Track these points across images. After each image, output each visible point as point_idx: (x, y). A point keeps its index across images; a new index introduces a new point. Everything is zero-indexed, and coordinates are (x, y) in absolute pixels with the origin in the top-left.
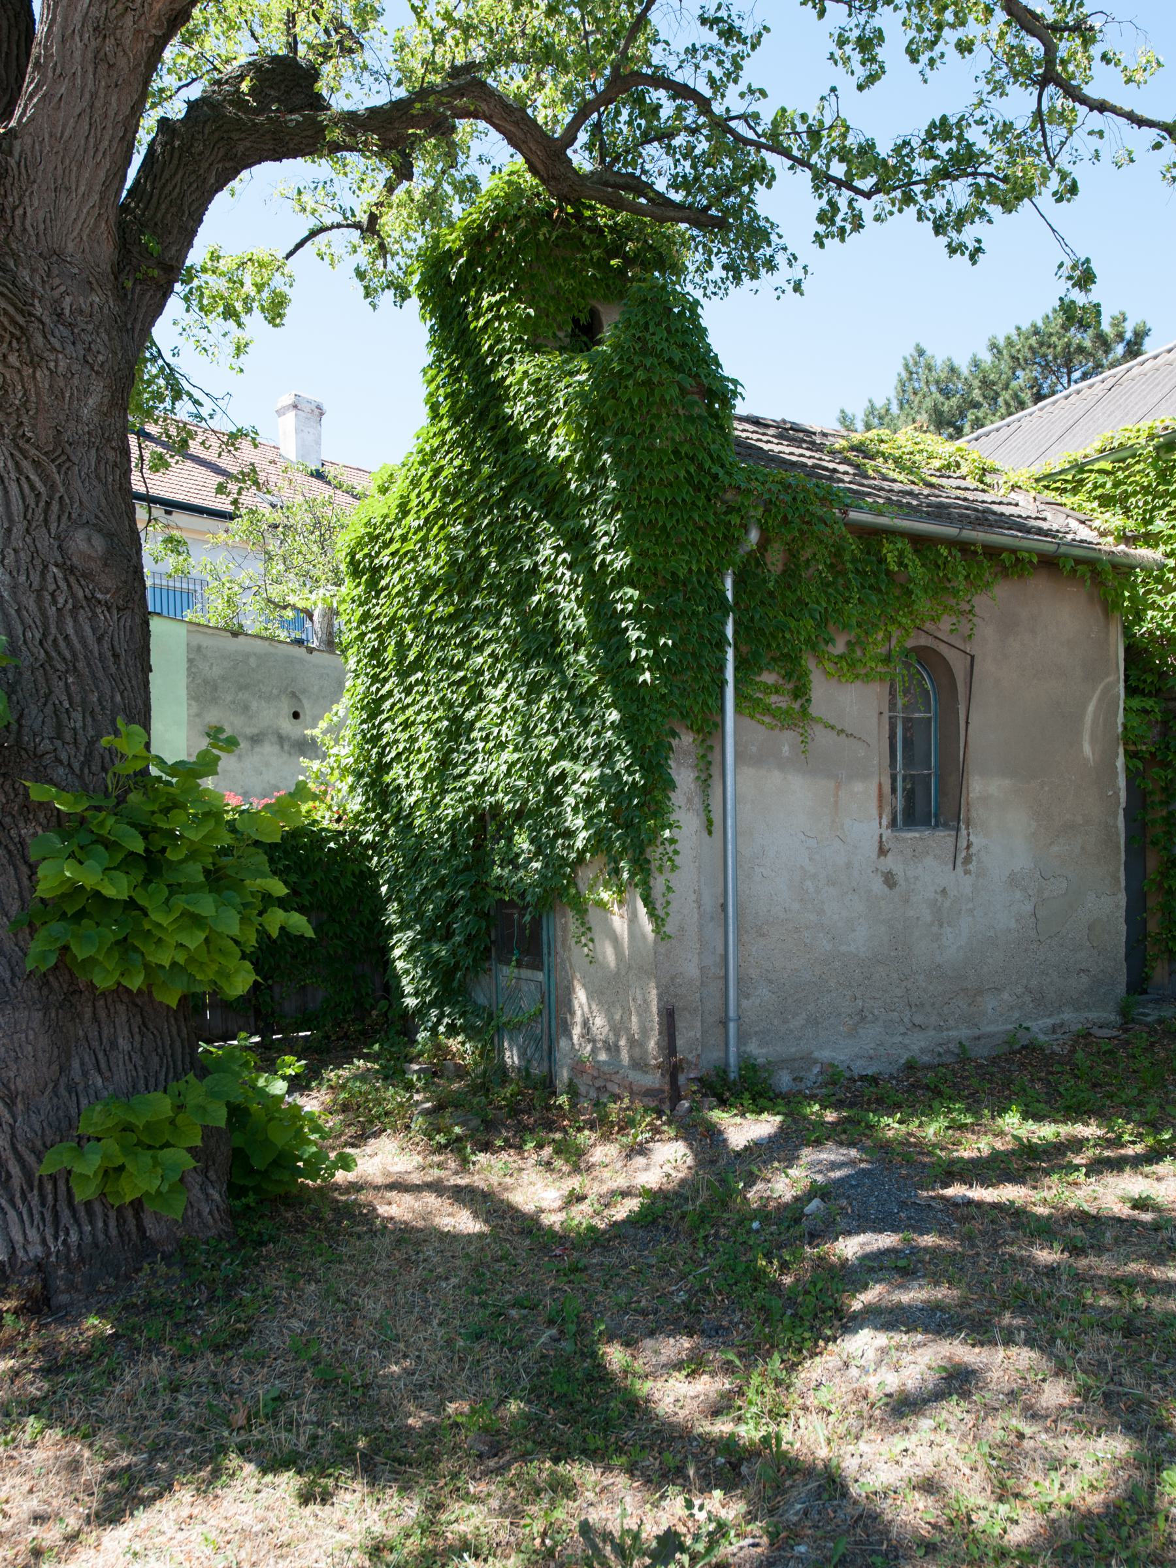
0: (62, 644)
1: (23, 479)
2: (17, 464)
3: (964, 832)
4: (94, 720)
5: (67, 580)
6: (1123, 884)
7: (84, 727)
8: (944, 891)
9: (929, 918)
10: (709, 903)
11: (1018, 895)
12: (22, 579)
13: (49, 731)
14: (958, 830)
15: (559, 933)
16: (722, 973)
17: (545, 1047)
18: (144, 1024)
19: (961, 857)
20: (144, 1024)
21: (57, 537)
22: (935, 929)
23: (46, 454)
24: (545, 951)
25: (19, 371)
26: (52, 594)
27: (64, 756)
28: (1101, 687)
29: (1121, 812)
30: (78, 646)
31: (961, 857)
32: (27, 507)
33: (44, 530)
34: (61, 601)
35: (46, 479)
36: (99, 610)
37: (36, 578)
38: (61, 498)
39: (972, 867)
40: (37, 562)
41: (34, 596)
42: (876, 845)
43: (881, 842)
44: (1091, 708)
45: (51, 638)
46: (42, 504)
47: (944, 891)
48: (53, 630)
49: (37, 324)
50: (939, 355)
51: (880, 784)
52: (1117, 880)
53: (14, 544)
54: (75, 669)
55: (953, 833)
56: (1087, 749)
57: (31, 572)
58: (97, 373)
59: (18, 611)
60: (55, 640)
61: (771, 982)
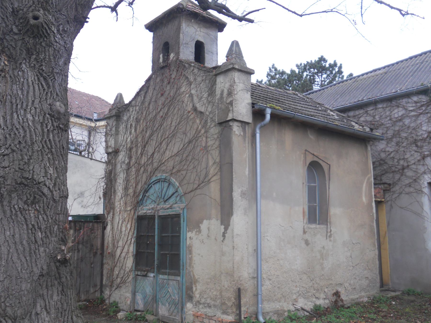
0: (48, 142)
1: (40, 83)
2: (38, 78)
3: (329, 226)
4: (57, 171)
5: (51, 120)
6: (377, 247)
7: (54, 173)
8: (323, 247)
9: (319, 257)
10: (251, 249)
11: (346, 249)
12: (37, 118)
13: (43, 174)
14: (327, 225)
15: (188, 261)
16: (256, 276)
17: (180, 307)
18: (63, 290)
19: (329, 235)
20: (63, 290)
21: (50, 104)
22: (321, 261)
23: (48, 76)
24: (181, 268)
25: (45, 48)
26: (46, 125)
27: (47, 183)
28: (367, 178)
29: (375, 221)
30: (53, 143)
31: (329, 235)
32: (40, 94)
33: (45, 102)
34: (49, 127)
35: (48, 84)
36: (60, 131)
37: (41, 118)
38: (51, 91)
39: (332, 239)
40: (42, 112)
41: (40, 124)
42: (302, 230)
43: (304, 229)
44: (364, 185)
45: (44, 140)
46: (45, 93)
47: (323, 247)
48: (46, 137)
49: (52, 33)
50: (280, 68)
51: (303, 209)
52: (375, 245)
53: (35, 106)
54: (51, 152)
55: (326, 226)
56: (364, 199)
57: (40, 116)
58: (66, 50)
59: (34, 130)
60: (45, 141)
61: (270, 280)
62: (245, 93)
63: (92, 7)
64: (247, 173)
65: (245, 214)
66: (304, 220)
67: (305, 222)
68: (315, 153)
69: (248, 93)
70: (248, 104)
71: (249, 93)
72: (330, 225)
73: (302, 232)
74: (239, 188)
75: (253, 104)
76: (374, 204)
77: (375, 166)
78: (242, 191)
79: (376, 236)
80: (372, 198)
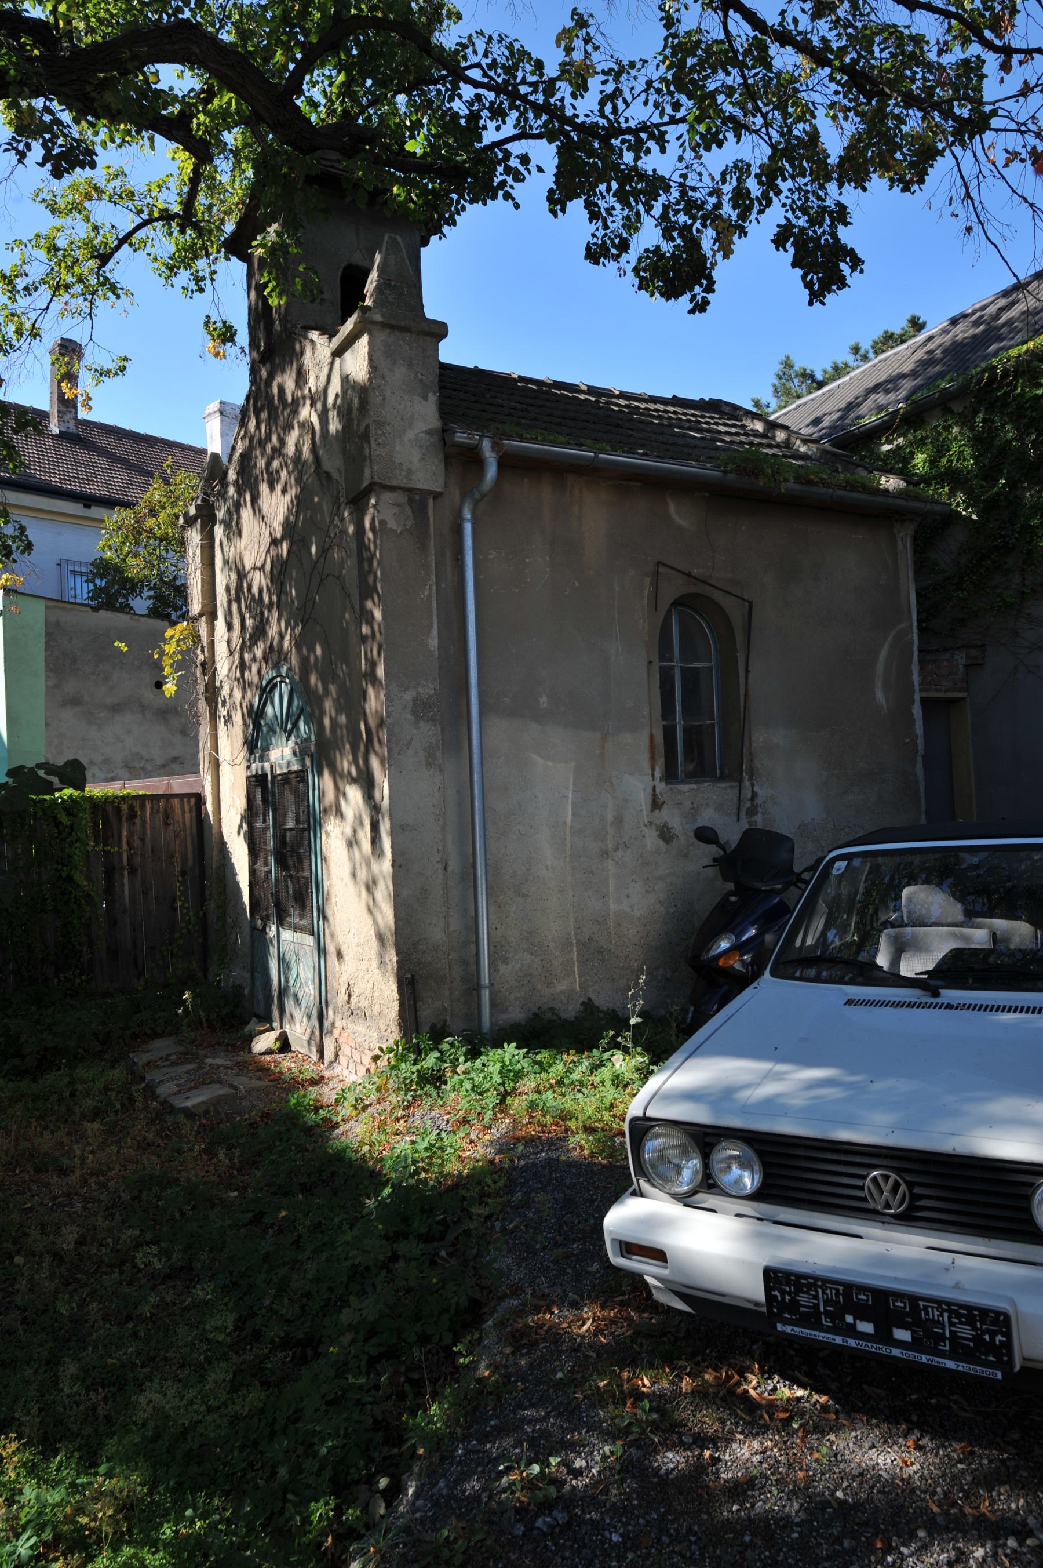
28: (893, 633)
29: (919, 759)
42: (650, 797)
43: (654, 795)
56: (880, 696)
62: (417, 399)
63: (364, 340)
64: (434, 643)
65: (429, 765)
66: (653, 770)
67: (658, 774)
68: (695, 572)
69: (426, 398)
70: (429, 433)
71: (433, 398)
72: (751, 779)
73: (649, 801)
74: (407, 689)
75: (444, 431)
76: (917, 710)
77: (427, 1014)
78: (415, 700)
79: (923, 801)
80: (914, 691)
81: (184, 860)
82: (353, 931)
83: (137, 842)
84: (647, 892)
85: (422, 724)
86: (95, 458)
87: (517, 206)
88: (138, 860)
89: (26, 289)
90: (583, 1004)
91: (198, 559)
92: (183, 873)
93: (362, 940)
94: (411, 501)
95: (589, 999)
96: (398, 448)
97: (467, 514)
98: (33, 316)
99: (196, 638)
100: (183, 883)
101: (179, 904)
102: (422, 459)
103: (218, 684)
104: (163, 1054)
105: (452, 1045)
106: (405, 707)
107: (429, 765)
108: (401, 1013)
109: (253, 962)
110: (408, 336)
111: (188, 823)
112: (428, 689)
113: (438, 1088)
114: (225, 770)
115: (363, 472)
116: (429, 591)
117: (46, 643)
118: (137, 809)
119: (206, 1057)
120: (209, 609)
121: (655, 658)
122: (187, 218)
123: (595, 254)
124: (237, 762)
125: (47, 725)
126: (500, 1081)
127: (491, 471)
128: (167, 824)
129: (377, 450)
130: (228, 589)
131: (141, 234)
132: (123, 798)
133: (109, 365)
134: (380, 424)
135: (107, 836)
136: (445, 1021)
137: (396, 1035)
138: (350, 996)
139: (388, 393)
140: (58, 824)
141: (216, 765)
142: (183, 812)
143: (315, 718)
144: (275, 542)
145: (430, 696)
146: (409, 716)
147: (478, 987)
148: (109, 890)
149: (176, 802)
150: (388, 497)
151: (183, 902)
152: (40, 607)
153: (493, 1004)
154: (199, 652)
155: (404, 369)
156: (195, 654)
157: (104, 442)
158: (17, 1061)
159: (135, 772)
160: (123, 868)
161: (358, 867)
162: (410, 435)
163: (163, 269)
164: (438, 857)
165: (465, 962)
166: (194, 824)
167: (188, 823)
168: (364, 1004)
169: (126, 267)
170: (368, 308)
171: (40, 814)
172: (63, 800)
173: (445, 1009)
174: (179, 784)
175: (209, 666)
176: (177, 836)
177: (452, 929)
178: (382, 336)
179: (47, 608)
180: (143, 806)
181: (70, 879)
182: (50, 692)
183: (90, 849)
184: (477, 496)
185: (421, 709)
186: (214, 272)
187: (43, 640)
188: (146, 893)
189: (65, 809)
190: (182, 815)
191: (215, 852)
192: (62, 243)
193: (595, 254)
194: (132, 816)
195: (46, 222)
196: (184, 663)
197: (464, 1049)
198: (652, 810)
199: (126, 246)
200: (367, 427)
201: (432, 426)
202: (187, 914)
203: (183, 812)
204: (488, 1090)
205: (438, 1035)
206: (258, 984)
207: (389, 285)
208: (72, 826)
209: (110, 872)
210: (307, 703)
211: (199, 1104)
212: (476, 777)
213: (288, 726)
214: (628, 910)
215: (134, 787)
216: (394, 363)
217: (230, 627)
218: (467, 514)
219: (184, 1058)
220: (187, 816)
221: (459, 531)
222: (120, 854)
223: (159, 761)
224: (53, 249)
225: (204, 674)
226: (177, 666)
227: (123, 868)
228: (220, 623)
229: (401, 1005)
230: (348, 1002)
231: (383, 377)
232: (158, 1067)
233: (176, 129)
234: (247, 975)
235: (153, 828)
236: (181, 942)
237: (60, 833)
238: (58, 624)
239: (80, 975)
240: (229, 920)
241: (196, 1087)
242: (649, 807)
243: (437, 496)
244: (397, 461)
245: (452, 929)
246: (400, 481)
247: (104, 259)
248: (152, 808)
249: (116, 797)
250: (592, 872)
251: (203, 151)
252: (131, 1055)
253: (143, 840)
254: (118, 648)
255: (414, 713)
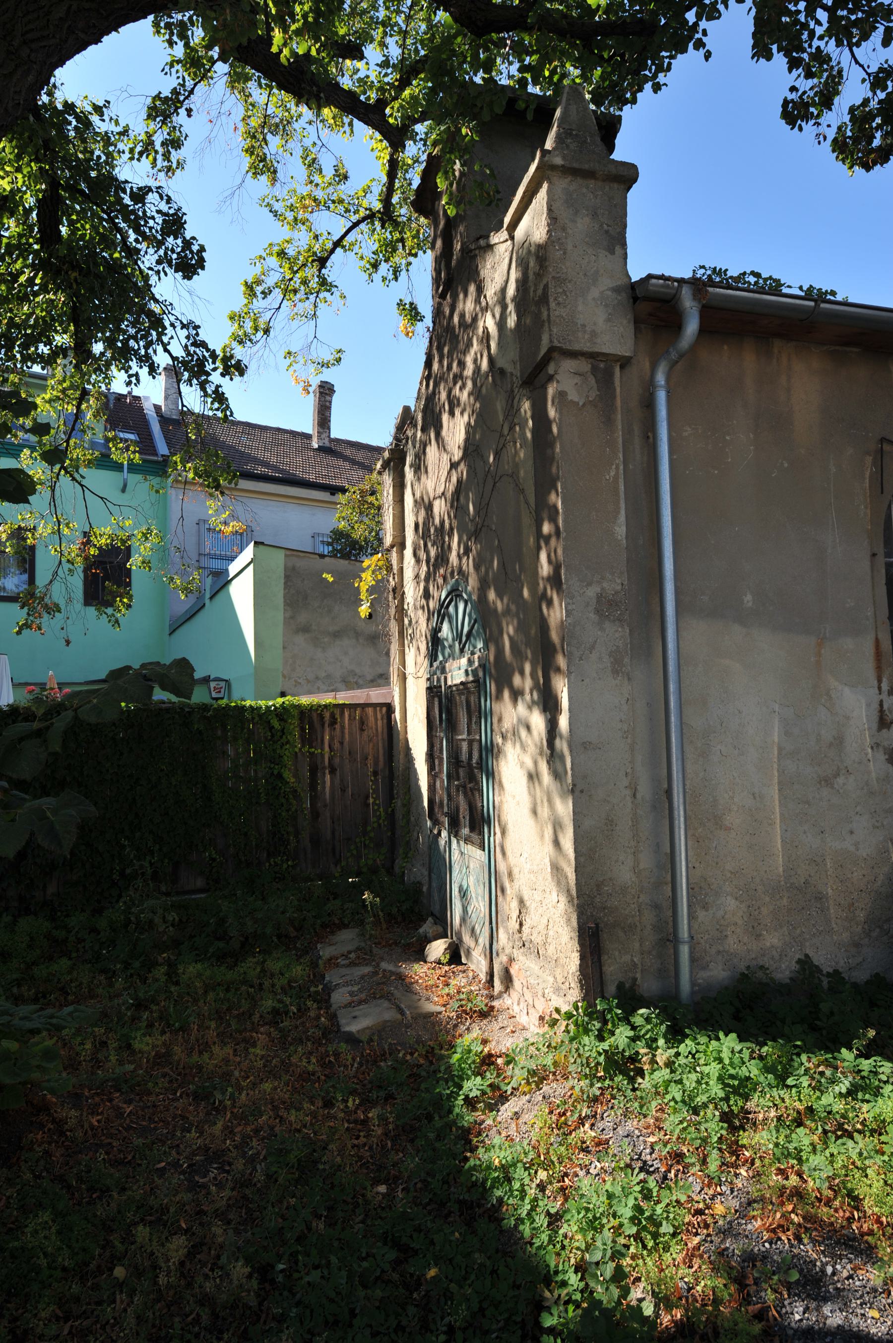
43: (881, 711)
64: (621, 530)
66: (880, 681)
74: (589, 584)
78: (599, 597)
81: (376, 762)
82: (525, 855)
83: (337, 745)
84: (875, 827)
85: (607, 625)
86: (341, 463)
87: (708, 56)
88: (337, 761)
89: (263, 293)
90: (799, 961)
91: (391, 498)
92: (375, 773)
93: (535, 868)
94: (594, 370)
95: (807, 956)
96: (580, 308)
97: (660, 378)
98: (268, 315)
99: (389, 568)
100: (375, 782)
101: (371, 800)
102: (608, 320)
103: (406, 607)
104: (345, 950)
105: (648, 1020)
106: (587, 605)
107: (615, 672)
108: (582, 968)
109: (430, 863)
110: (592, 183)
111: (380, 729)
112: (614, 584)
113: (632, 1080)
114: (410, 681)
115: (540, 339)
116: (615, 472)
117: (285, 583)
118: (338, 716)
119: (382, 959)
120: (398, 540)
121: (881, 550)
122: (387, 216)
123: (795, 113)
124: (420, 674)
125: (284, 648)
126: (721, 1094)
127: (692, 327)
128: (362, 730)
129: (556, 311)
130: (417, 525)
131: (350, 238)
132: (326, 706)
133: (328, 357)
134: (560, 281)
135: (310, 739)
136: (635, 979)
137: (575, 994)
138: (521, 925)
139: (570, 247)
140: (271, 728)
141: (403, 678)
142: (376, 719)
143: (493, 639)
144: (454, 466)
145: (617, 593)
146: (592, 616)
147: (675, 940)
148: (313, 785)
149: (370, 711)
150: (568, 365)
151: (375, 799)
152: (280, 556)
153: (693, 960)
154: (391, 579)
155: (587, 220)
156: (388, 581)
157: (348, 452)
158: (221, 944)
159: (349, 684)
160: (324, 768)
161: (539, 801)
162: (595, 293)
163: (368, 266)
164: (625, 782)
165: (657, 907)
166: (385, 730)
167: (380, 729)
168: (537, 939)
169: (340, 267)
170: (549, 152)
171: (257, 719)
172: (276, 708)
173: (635, 965)
174: (375, 695)
175: (399, 592)
176: (370, 741)
177: (642, 866)
178: (563, 183)
179: (286, 556)
180: (342, 714)
181: (280, 776)
182: (287, 621)
183: (297, 750)
184: (674, 355)
185: (606, 607)
186: (409, 264)
187: (283, 581)
188: (343, 790)
189: (277, 715)
190: (376, 722)
191: (402, 756)
192: (291, 252)
193: (795, 113)
194: (333, 722)
195: (279, 233)
196: (377, 589)
197: (663, 1028)
198: (880, 729)
199: (339, 250)
200: (546, 286)
201: (619, 283)
202: (378, 810)
203: (376, 719)
204: (705, 1106)
205: (630, 1001)
206: (434, 885)
207: (571, 134)
208: (283, 731)
209: (314, 770)
210: (486, 621)
211: (364, 1030)
212: (672, 687)
213: (463, 640)
214: (852, 849)
215: (343, 697)
216: (577, 212)
217: (418, 561)
218: (660, 378)
219: (363, 956)
220: (380, 723)
221: (649, 405)
222: (322, 755)
223: (369, 677)
224: (282, 254)
225: (395, 598)
226: (371, 590)
227: (324, 768)
228: (408, 552)
229: (582, 958)
230: (520, 931)
231: (564, 229)
232: (337, 965)
233: (372, 115)
234: (426, 873)
235: (350, 733)
236: (372, 835)
237: (272, 736)
238: (294, 568)
239: (288, 860)
240: (412, 819)
241: (365, 1001)
242: (875, 726)
243: (625, 362)
244: (580, 322)
245: (642, 866)
246: (582, 344)
247: (322, 262)
248: (350, 716)
249: (320, 706)
250: (808, 803)
251: (396, 137)
252: (319, 946)
253: (342, 743)
254: (326, 579)
255: (597, 611)
